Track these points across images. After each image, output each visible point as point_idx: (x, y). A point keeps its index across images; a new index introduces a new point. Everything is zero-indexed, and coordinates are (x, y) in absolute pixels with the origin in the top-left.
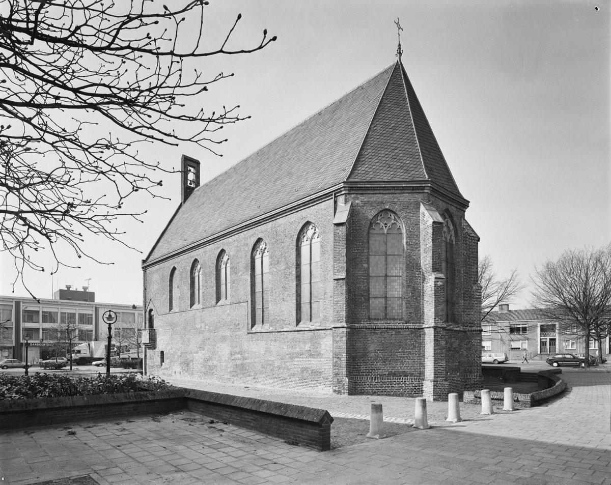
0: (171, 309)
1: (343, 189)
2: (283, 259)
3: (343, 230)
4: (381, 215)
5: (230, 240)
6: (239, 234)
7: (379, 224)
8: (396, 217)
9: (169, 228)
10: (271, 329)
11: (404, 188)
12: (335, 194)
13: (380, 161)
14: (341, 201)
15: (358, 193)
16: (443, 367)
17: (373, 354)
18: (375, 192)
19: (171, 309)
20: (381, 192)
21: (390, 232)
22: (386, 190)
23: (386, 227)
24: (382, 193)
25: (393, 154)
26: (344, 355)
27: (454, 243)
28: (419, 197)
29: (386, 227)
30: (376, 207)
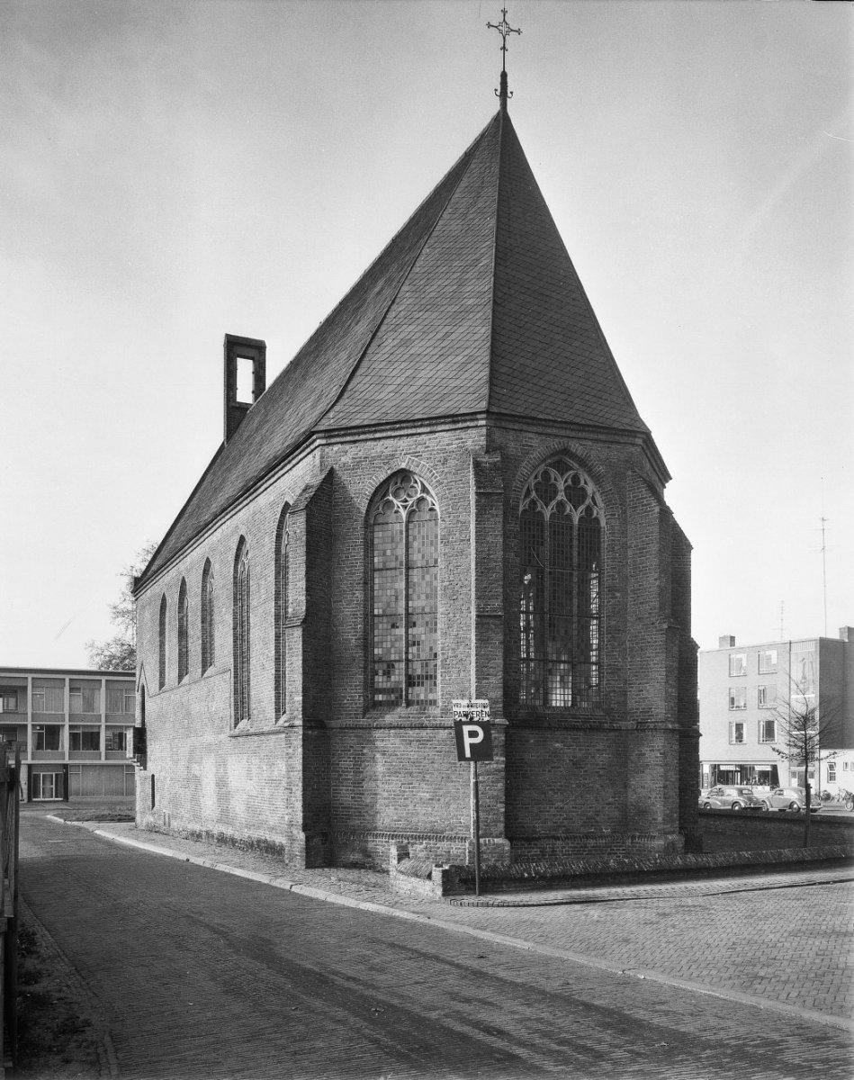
0: (162, 685)
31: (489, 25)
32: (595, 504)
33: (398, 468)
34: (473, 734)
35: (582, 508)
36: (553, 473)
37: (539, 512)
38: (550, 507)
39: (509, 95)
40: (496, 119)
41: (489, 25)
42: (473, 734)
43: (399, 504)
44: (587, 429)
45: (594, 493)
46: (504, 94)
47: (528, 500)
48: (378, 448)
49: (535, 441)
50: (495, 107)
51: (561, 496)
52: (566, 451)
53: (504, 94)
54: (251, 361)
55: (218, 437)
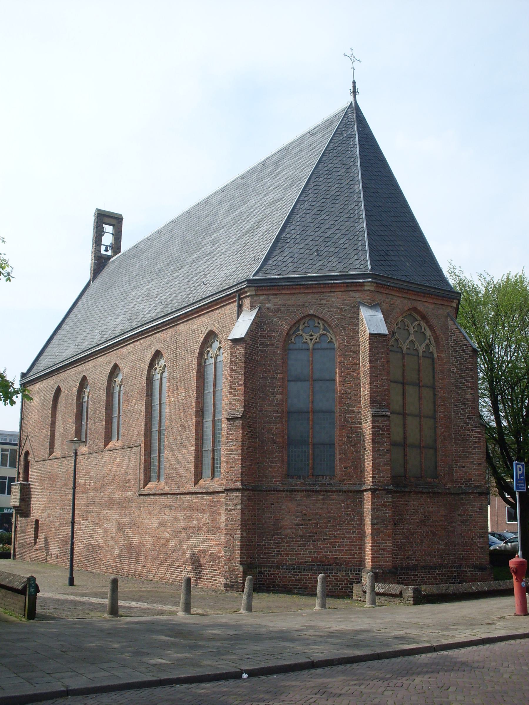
0: (51, 452)
1: (246, 289)
2: (182, 384)
3: (241, 349)
4: (304, 323)
5: (124, 350)
6: (135, 343)
7: (302, 335)
8: (326, 325)
9: (66, 321)
10: (167, 489)
11: (332, 286)
12: (239, 296)
13: (307, 247)
14: (247, 305)
15: (269, 294)
16: (388, 551)
17: (289, 530)
18: (294, 292)
19: (51, 452)
20: (302, 291)
21: (316, 346)
22: (308, 288)
23: (311, 340)
24: (303, 293)
25: (327, 235)
26: (238, 531)
27: (435, 356)
28: (357, 296)
29: (311, 340)
33: (307, 313)
36: (407, 321)
39: (357, 93)
43: (308, 337)
44: (427, 295)
45: (430, 336)
46: (355, 92)
47: (393, 339)
48: (301, 299)
52: (415, 309)
53: (355, 92)
54: (112, 227)
55: (87, 277)
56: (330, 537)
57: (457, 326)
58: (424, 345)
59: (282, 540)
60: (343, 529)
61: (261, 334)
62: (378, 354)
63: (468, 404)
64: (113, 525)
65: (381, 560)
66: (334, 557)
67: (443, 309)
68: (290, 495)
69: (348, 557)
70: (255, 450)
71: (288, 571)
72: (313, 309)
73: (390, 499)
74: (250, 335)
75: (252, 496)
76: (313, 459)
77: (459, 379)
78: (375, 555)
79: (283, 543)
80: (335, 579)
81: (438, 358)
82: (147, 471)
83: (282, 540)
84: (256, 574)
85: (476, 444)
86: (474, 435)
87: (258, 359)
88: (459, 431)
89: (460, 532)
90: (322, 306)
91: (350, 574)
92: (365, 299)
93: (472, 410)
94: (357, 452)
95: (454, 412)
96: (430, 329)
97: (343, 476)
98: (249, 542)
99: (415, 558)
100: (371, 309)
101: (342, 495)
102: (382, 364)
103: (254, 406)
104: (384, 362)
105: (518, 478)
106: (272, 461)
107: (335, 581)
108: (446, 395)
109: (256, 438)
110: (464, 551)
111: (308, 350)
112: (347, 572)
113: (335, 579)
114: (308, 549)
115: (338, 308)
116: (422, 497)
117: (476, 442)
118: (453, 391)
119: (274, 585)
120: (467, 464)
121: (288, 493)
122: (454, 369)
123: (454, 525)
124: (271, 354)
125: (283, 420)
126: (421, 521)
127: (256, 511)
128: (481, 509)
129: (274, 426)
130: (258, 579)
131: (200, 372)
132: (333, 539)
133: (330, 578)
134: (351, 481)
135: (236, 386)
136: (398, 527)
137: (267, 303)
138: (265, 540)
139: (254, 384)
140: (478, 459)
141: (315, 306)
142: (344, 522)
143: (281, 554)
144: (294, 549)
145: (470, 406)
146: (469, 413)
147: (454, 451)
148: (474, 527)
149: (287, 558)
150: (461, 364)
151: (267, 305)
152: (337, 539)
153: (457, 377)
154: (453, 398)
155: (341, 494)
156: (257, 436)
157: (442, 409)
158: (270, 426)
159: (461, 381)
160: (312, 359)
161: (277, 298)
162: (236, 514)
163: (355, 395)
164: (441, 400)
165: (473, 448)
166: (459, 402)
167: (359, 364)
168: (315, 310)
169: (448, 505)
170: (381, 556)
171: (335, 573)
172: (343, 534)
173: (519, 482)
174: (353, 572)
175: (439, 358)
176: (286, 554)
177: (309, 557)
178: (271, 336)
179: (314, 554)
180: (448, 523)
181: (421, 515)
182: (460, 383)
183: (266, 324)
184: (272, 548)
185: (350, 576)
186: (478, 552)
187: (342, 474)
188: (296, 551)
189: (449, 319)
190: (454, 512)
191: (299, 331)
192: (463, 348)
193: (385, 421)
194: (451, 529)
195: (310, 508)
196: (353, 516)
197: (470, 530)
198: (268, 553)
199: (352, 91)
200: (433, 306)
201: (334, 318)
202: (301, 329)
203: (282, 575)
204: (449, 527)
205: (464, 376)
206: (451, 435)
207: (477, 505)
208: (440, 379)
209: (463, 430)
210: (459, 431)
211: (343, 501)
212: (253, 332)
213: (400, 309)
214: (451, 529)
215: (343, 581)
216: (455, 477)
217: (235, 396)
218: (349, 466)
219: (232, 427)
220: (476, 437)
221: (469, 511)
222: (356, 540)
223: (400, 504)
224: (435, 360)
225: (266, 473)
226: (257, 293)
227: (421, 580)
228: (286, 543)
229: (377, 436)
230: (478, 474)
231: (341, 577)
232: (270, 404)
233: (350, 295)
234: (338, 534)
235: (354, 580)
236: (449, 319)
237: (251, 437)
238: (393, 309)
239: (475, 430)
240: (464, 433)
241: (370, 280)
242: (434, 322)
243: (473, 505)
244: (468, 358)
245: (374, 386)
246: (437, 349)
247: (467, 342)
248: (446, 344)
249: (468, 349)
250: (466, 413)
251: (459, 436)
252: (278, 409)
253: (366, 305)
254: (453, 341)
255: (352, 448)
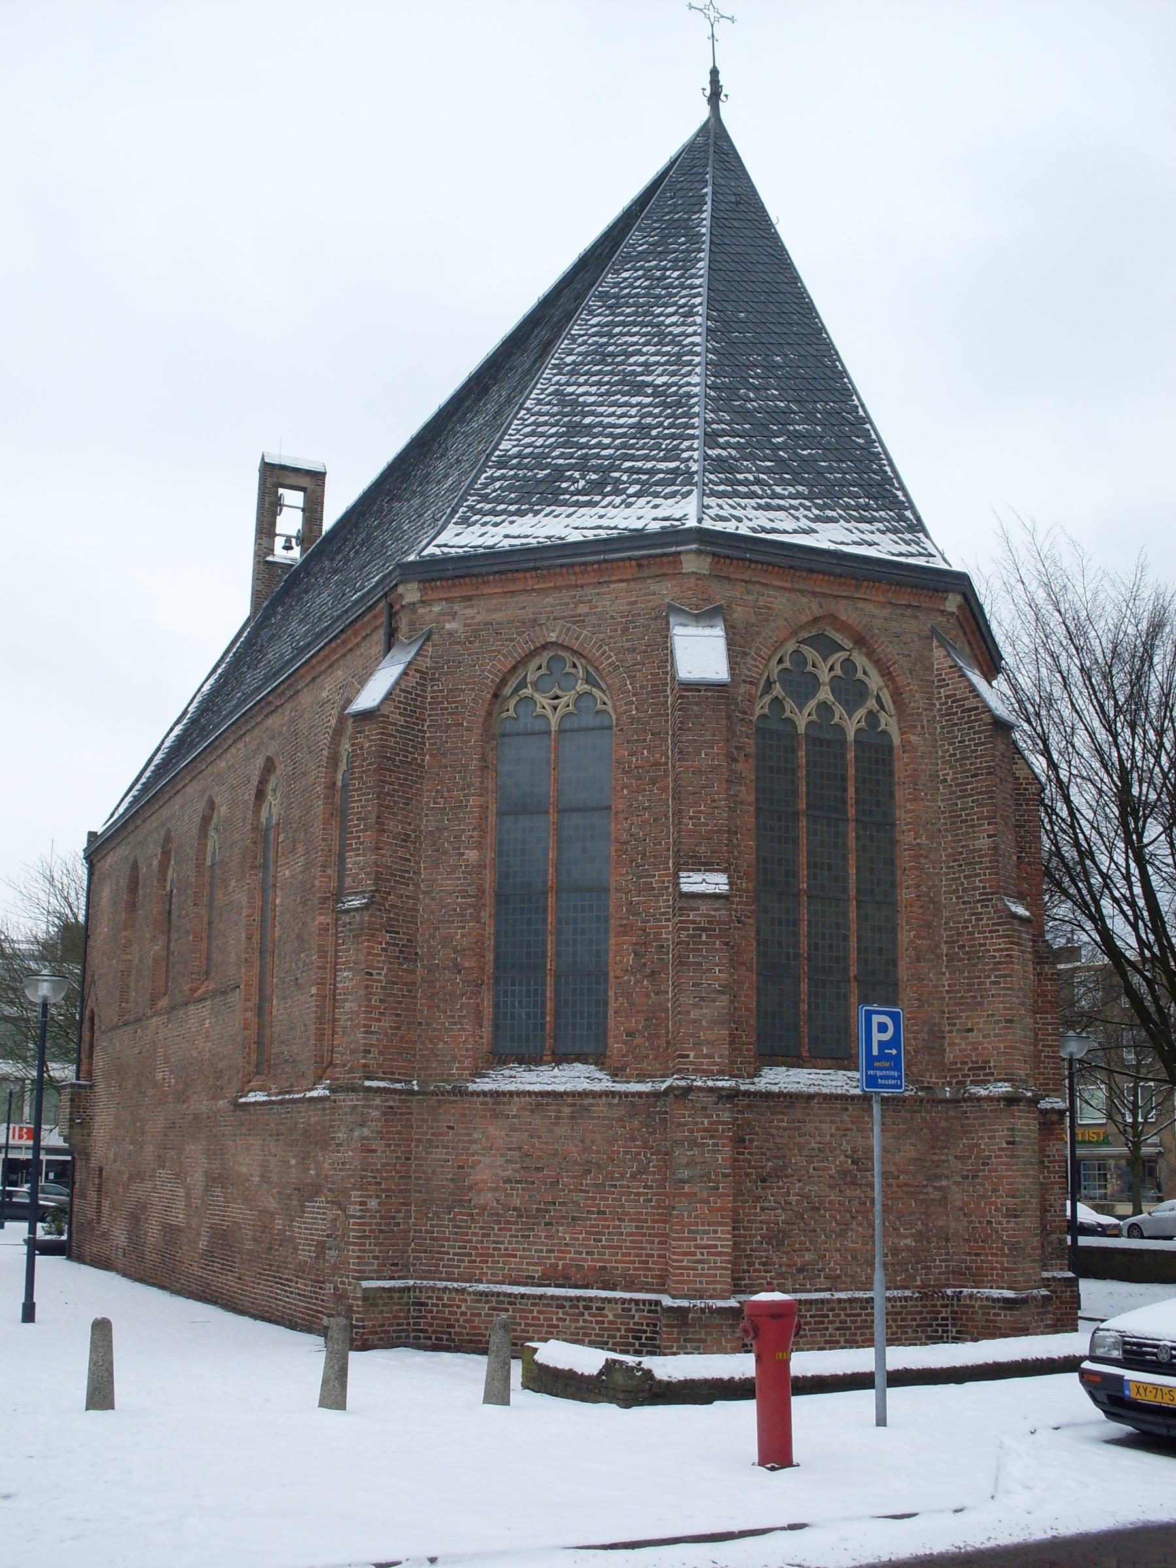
2: (302, 836)
16: (719, 1254)
17: (490, 1195)
21: (567, 725)
28: (665, 591)
30: (512, 640)
31: (691, 7)
32: (882, 708)
34: (883, 1028)
35: (861, 713)
36: (810, 653)
37: (788, 719)
38: (806, 711)
40: (704, 129)
41: (732, 19)
42: (883, 1028)
43: (545, 702)
45: (880, 689)
46: (715, 96)
47: (767, 699)
49: (780, 602)
50: (703, 113)
51: (825, 694)
52: (833, 619)
53: (715, 96)
56: (588, 1212)
57: (954, 660)
58: (861, 713)
59: (473, 1221)
60: (621, 1194)
61: (431, 698)
62: (702, 735)
63: (981, 863)
64: (197, 1179)
65: (700, 1275)
66: (598, 1265)
67: (917, 617)
68: (493, 1104)
69: (631, 1266)
70: (410, 991)
71: (484, 1298)
72: (558, 630)
73: (726, 1116)
74: (400, 702)
75: (398, 1108)
76: (557, 1014)
77: (959, 798)
78: (685, 1263)
79: (475, 1227)
80: (597, 1322)
81: (903, 746)
82: (250, 1048)
83: (473, 1221)
84: (408, 1304)
85: (999, 970)
86: (995, 944)
87: (423, 760)
88: (958, 934)
89: (958, 1203)
90: (578, 622)
91: (633, 1312)
92: (685, 598)
93: (990, 880)
94: (657, 994)
95: (946, 886)
96: (879, 671)
97: (624, 1056)
98: (386, 1225)
99: (823, 1270)
100: (697, 621)
101: (618, 1105)
102: (713, 759)
103: (410, 879)
104: (718, 755)
105: (875, 1052)
106: (453, 1017)
107: (597, 1327)
108: (923, 840)
109: (416, 961)
110: (969, 1254)
111: (548, 733)
112: (626, 1306)
113: (597, 1322)
114: (534, 1243)
115: (618, 624)
116: (847, 1109)
117: (1000, 963)
118: (946, 830)
119: (450, 1333)
120: (978, 1023)
121: (488, 1099)
122: (948, 774)
123: (944, 1183)
124: (456, 748)
125: (482, 914)
126: (844, 1173)
127: (413, 1144)
128: (1012, 1143)
129: (458, 928)
130: (413, 1317)
131: (332, 803)
132: (595, 1219)
133: (585, 1321)
134: (641, 1069)
135: (361, 831)
136: (771, 1188)
137: (449, 622)
138: (431, 1219)
139: (410, 824)
140: (1005, 1009)
141: (561, 622)
142: (623, 1176)
143: (470, 1255)
144: (502, 1243)
145: (987, 868)
146: (984, 888)
147: (947, 988)
148: (994, 1191)
149: (484, 1266)
150: (963, 759)
151: (448, 626)
152: (606, 1220)
153: (954, 793)
154: (945, 849)
155: (616, 1101)
156: (416, 954)
157: (912, 880)
158: (450, 928)
159: (963, 803)
160: (557, 757)
161: (472, 607)
162: (350, 1153)
163: (655, 844)
164: (909, 855)
165: (993, 979)
166: (958, 860)
167: (666, 764)
168: (561, 632)
169: (924, 1130)
170: (700, 1266)
171: (598, 1308)
172: (622, 1206)
173: (877, 1064)
174: (642, 1307)
175: (905, 744)
176: (482, 1255)
177: (535, 1264)
178: (455, 702)
179: (549, 1258)
180: (928, 1179)
181: (842, 1158)
182: (962, 809)
183: (445, 674)
184: (448, 1240)
185: (633, 1317)
186: (1004, 1255)
187: (620, 1049)
188: (506, 1249)
189: (935, 643)
190: (946, 1151)
191: (526, 687)
192: (970, 716)
193: (716, 910)
194: (936, 1195)
195: (539, 1137)
196: (646, 1158)
197: (983, 1197)
198: (438, 1253)
199: (708, 93)
200: (886, 612)
201: (607, 648)
202: (531, 683)
203: (468, 1308)
204: (930, 1189)
205: (972, 789)
206: (938, 946)
207: (1003, 1131)
208: (908, 800)
209: (969, 933)
210: (958, 934)
211: (620, 1119)
212: (411, 693)
213: (785, 619)
214: (936, 1195)
215: (619, 1330)
216: (949, 1059)
217: (359, 855)
218: (638, 1031)
219: (348, 933)
220: (1002, 950)
221: (982, 1147)
222: (654, 1221)
223: (778, 1128)
224: (895, 751)
225: (439, 1050)
226: (425, 598)
227: (838, 1329)
228: (482, 1228)
229: (693, 950)
230: (1005, 1048)
231: (611, 1317)
232: (450, 873)
233: (648, 588)
234: (608, 1206)
235: (645, 1328)
236: (935, 643)
237: (398, 958)
238: (767, 620)
239: (998, 931)
240: (971, 940)
241: (694, 546)
242: (889, 650)
243: (992, 1131)
244: (982, 744)
245: (691, 818)
246: (899, 722)
247: (978, 702)
248: (926, 709)
249: (981, 720)
250: (975, 889)
251: (960, 947)
252: (469, 885)
253: (683, 611)
254: (943, 700)
255: (645, 982)
